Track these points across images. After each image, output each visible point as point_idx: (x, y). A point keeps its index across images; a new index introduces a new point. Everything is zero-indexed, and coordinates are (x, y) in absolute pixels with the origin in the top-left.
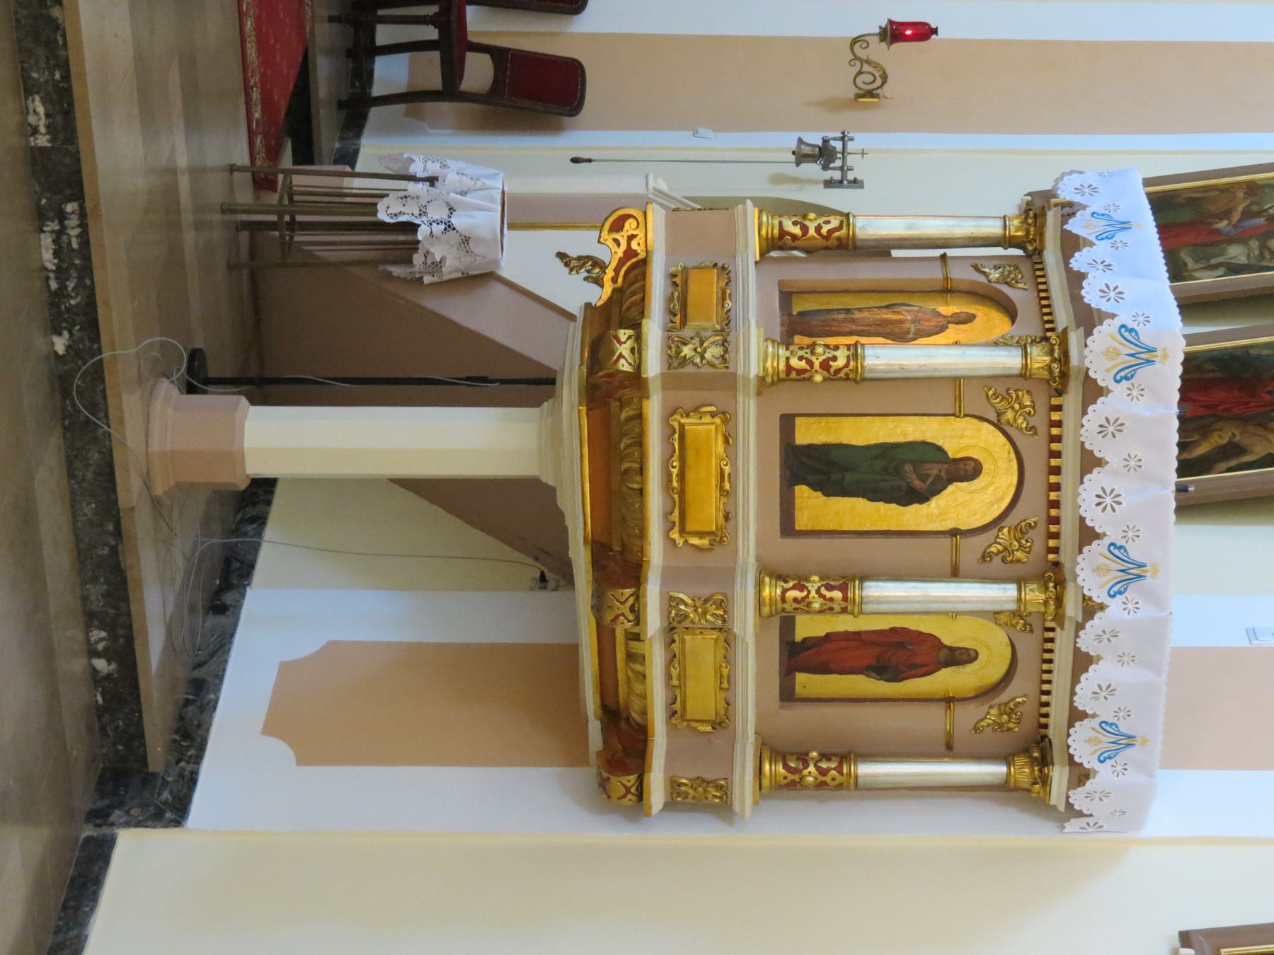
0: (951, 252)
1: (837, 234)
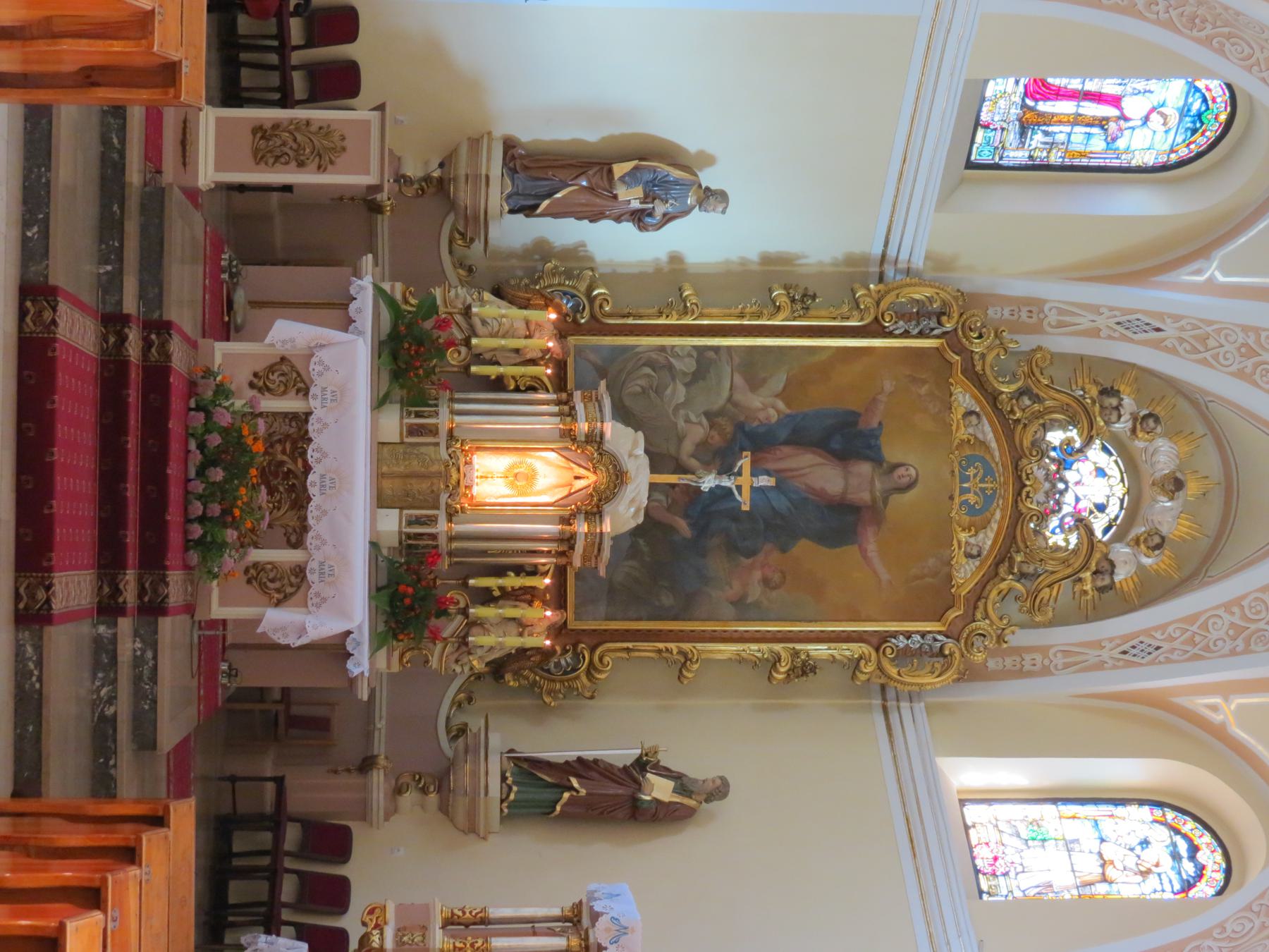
0: (536, 925)
1: (480, 915)
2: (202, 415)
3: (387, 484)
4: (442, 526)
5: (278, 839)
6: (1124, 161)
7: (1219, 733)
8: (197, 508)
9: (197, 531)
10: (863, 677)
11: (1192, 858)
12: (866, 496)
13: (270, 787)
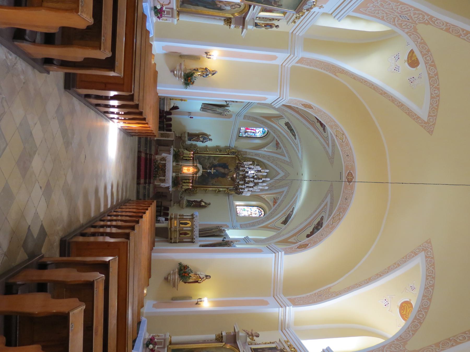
2: (155, 163)
3: (174, 170)
4: (180, 175)
5: (161, 208)
6: (256, 137)
7: (264, 199)
8: (154, 173)
9: (154, 175)
10: (226, 192)
11: (261, 212)
12: (227, 173)
13: (160, 203)
